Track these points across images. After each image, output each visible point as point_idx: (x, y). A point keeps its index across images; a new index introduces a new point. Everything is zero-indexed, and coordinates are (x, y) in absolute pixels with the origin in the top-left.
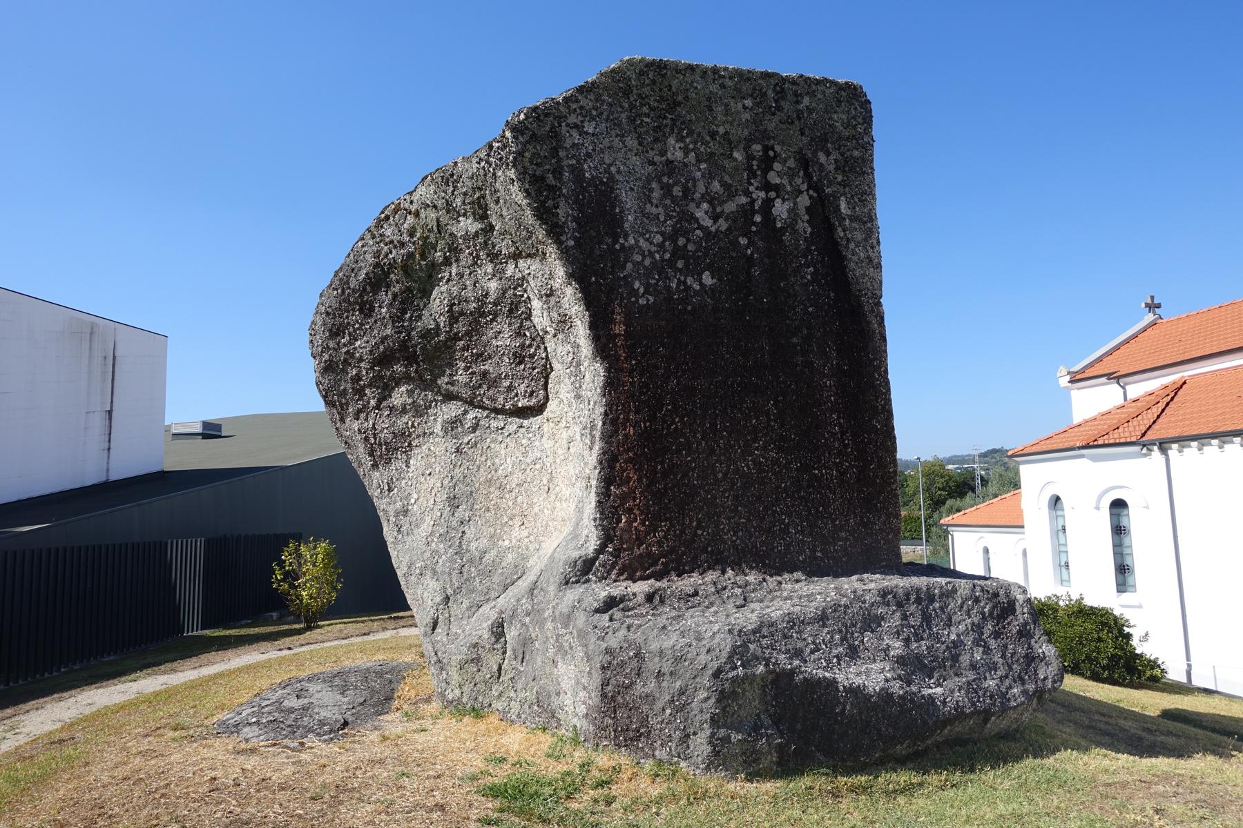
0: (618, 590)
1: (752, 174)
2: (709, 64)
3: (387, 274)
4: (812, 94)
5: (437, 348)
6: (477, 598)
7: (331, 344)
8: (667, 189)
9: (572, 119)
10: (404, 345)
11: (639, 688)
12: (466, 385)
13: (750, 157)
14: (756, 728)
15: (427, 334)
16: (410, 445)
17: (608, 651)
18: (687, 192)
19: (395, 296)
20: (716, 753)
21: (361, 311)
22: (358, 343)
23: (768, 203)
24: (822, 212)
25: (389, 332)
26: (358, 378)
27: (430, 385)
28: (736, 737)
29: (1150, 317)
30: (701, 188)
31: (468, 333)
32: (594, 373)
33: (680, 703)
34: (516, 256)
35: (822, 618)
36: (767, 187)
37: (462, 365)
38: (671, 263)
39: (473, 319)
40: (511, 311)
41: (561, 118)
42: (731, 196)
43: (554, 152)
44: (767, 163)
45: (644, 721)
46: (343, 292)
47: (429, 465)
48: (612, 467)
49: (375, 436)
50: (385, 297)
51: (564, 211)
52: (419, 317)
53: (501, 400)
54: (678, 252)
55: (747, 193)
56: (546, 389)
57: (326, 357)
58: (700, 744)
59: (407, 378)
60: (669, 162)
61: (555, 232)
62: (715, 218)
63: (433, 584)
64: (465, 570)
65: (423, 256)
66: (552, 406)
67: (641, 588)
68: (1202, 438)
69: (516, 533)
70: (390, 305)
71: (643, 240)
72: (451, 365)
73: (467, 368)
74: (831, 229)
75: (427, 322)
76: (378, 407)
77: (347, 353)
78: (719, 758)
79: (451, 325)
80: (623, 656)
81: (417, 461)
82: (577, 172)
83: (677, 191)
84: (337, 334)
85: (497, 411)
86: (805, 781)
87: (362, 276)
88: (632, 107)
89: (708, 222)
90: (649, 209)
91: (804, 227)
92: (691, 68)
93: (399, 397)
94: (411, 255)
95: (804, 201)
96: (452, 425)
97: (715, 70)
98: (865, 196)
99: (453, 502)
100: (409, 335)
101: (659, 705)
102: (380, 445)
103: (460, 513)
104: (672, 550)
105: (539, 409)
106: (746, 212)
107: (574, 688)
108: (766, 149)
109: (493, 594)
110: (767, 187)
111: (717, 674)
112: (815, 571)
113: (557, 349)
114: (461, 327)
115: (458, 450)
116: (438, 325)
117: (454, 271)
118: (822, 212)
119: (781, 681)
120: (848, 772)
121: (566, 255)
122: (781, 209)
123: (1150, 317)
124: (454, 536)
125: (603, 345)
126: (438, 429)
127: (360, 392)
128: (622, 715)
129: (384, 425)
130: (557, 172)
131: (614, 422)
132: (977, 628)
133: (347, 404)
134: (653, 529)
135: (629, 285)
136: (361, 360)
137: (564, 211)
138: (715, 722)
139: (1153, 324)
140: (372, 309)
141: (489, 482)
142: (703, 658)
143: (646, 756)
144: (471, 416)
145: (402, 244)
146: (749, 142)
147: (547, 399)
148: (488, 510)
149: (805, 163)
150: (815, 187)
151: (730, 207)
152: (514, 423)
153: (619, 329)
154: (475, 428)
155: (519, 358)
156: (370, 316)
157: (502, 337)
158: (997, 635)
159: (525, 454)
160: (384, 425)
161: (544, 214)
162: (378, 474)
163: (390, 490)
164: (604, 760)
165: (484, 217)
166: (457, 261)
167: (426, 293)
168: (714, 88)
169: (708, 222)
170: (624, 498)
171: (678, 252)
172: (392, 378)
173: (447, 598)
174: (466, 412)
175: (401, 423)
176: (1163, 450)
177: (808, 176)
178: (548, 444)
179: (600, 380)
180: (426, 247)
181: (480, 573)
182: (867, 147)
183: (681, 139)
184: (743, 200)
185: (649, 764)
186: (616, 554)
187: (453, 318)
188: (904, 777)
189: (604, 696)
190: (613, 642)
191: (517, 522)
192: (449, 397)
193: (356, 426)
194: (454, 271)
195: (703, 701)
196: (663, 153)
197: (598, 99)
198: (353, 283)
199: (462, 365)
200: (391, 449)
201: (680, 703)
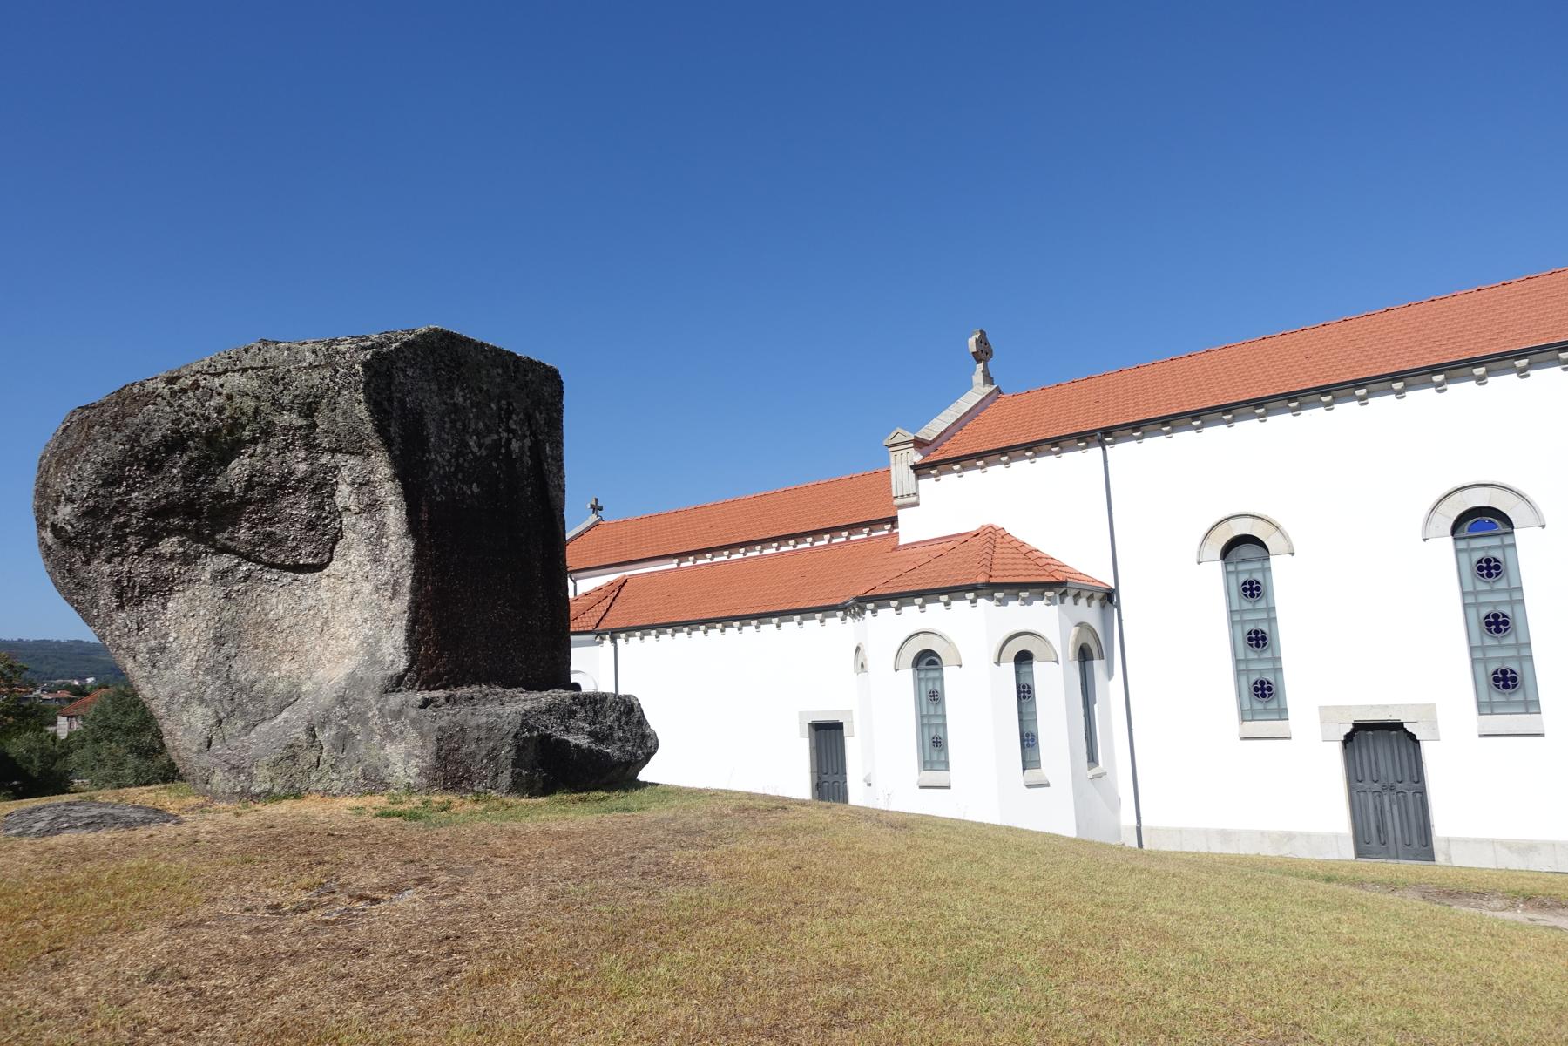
0: (427, 694)
1: (501, 420)
2: (478, 339)
3: (185, 441)
4: (533, 371)
5: (226, 508)
6: (251, 719)
7: (101, 492)
8: (453, 422)
9: (400, 364)
10: (191, 503)
11: (464, 749)
12: (247, 542)
13: (500, 409)
14: (533, 768)
15: (219, 496)
16: (171, 589)
17: (440, 729)
18: (465, 426)
19: (192, 460)
20: (514, 783)
21: (147, 467)
22: (134, 495)
23: (509, 441)
24: (536, 450)
25: (177, 489)
26: (125, 525)
27: (209, 540)
28: (525, 773)
29: (593, 518)
30: (473, 426)
31: (261, 500)
32: (399, 549)
33: (493, 756)
34: (333, 451)
35: (549, 711)
36: (509, 430)
37: (246, 525)
38: (455, 474)
39: (272, 491)
40: (314, 489)
41: (393, 362)
42: (489, 433)
43: (389, 385)
44: (509, 413)
45: (468, 769)
46: (132, 448)
47: (193, 608)
48: (417, 612)
49: (129, 580)
50: (181, 460)
51: (394, 429)
52: (214, 481)
53: (282, 557)
54: (459, 467)
55: (498, 433)
56: (331, 551)
57: (91, 502)
58: (505, 778)
59: (180, 531)
60: (455, 404)
61: (388, 443)
62: (480, 446)
63: (200, 711)
64: (236, 698)
65: (230, 433)
66: (336, 566)
67: (439, 694)
68: (645, 629)
69: (286, 666)
70: (184, 467)
71: (440, 459)
72: (234, 524)
73: (250, 529)
74: (541, 464)
75: (221, 484)
76: (139, 553)
77: (120, 502)
78: (517, 787)
79: (246, 492)
80: (452, 731)
81: (176, 604)
82: (402, 403)
83: (459, 424)
84: (112, 484)
85: (272, 566)
86: (558, 797)
87: (157, 437)
88: (435, 362)
89: (476, 449)
90: (444, 436)
91: (527, 460)
92: (469, 341)
93: (169, 545)
94: (217, 430)
95: (527, 442)
96: (222, 576)
97: (482, 345)
98: (558, 444)
99: (219, 641)
100: (199, 495)
101: (479, 758)
102: (134, 587)
103: (225, 650)
104: (452, 671)
105: (320, 567)
106: (497, 445)
107: (404, 759)
108: (509, 404)
109: (268, 715)
110: (509, 430)
111: (515, 737)
112: (529, 688)
113: (355, 528)
114: (256, 494)
115: (227, 597)
116: (232, 490)
117: (259, 449)
118: (536, 450)
119: (544, 739)
120: (576, 792)
121: (395, 461)
122: (515, 445)
123: (593, 518)
124: (219, 669)
125: (414, 526)
126: (207, 576)
127: (122, 539)
128: (451, 770)
129: (142, 569)
130: (390, 400)
131: (419, 581)
132: (618, 719)
133: (100, 548)
134: (440, 656)
135: (431, 486)
136: (135, 509)
137: (394, 429)
138: (514, 765)
139: (596, 525)
140: (161, 467)
141: (258, 624)
142: (507, 727)
143: (467, 792)
144: (244, 568)
145: (208, 419)
146: (500, 398)
147: (331, 559)
148: (256, 647)
149: (529, 418)
150: (534, 434)
151: (488, 441)
152: (288, 577)
153: (425, 517)
154: (246, 578)
155: (311, 525)
156: (157, 473)
157: (301, 507)
158: (627, 723)
159: (299, 601)
160: (142, 569)
161: (381, 429)
162: (123, 615)
163: (139, 629)
164: (437, 799)
165: (309, 416)
166: (266, 442)
167: (225, 462)
168: (481, 357)
169: (476, 449)
170: (424, 634)
171: (459, 467)
172: (164, 529)
173: (220, 721)
174: (239, 564)
175: (165, 569)
176: (613, 640)
177: (530, 426)
178: (325, 595)
179: (409, 552)
180: (236, 425)
181: (251, 699)
182: (560, 411)
183: (462, 390)
184: (495, 437)
185: (469, 796)
186: (418, 673)
187: (250, 486)
188: (601, 794)
189: (438, 757)
190: (443, 723)
191: (287, 657)
192: (222, 550)
193: (107, 568)
194: (259, 449)
195: (507, 752)
196: (452, 397)
197: (415, 353)
198: (144, 441)
199: (246, 525)
200: (145, 593)
201: (493, 756)
